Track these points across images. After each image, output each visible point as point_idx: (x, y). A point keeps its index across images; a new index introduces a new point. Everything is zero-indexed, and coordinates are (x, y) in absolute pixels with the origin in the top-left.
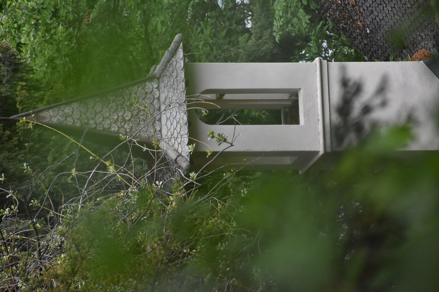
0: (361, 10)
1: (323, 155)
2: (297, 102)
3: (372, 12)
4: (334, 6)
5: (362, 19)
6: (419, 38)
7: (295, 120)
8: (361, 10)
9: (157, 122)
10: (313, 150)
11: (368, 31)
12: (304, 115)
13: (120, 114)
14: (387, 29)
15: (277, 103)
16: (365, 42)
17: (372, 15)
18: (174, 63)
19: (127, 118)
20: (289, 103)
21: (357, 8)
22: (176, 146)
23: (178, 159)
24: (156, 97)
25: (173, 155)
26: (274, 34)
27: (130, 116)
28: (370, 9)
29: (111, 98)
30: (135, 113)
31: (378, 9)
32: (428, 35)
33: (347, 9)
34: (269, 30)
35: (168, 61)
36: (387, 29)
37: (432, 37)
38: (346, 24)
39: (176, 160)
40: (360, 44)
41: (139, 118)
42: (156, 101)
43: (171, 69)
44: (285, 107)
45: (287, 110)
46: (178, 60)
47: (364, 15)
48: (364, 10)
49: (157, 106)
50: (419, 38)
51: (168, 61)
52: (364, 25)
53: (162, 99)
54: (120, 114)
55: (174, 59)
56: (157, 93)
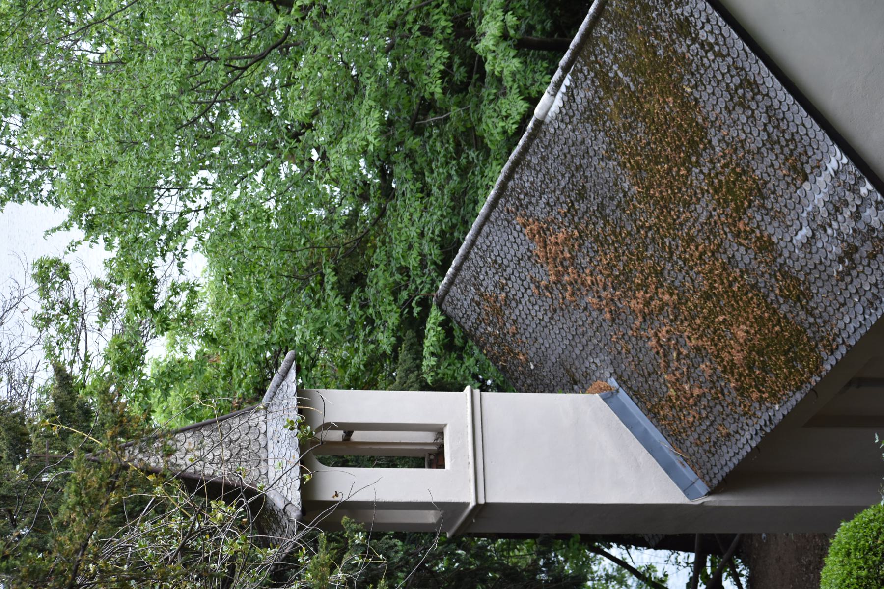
0: (524, 339)
1: (475, 508)
2: (442, 446)
3: (536, 339)
4: (491, 339)
5: (524, 350)
6: (593, 367)
7: (442, 466)
8: (524, 339)
9: (262, 463)
10: (461, 500)
11: (532, 367)
12: (451, 457)
13: (217, 453)
14: (554, 361)
15: (419, 447)
16: (529, 382)
17: (536, 344)
18: (285, 388)
19: (226, 458)
20: (434, 448)
21: (518, 336)
22: (285, 492)
23: (287, 508)
24: (263, 431)
25: (280, 504)
26: (425, 376)
27: (229, 455)
28: (533, 335)
29: (206, 434)
30: (235, 451)
31: (543, 334)
32: (604, 360)
33: (506, 340)
34: (416, 373)
35: (278, 386)
36: (554, 361)
37: (609, 362)
38: (506, 361)
39: (284, 509)
40: (523, 386)
41: (240, 458)
42: (262, 436)
43: (281, 395)
44: (430, 454)
45: (432, 457)
46: (290, 384)
47: (526, 345)
48: (526, 338)
49: (263, 444)
50: (593, 367)
51: (278, 386)
52: (527, 359)
53: (269, 434)
54: (217, 453)
55: (284, 383)
56: (264, 426)
